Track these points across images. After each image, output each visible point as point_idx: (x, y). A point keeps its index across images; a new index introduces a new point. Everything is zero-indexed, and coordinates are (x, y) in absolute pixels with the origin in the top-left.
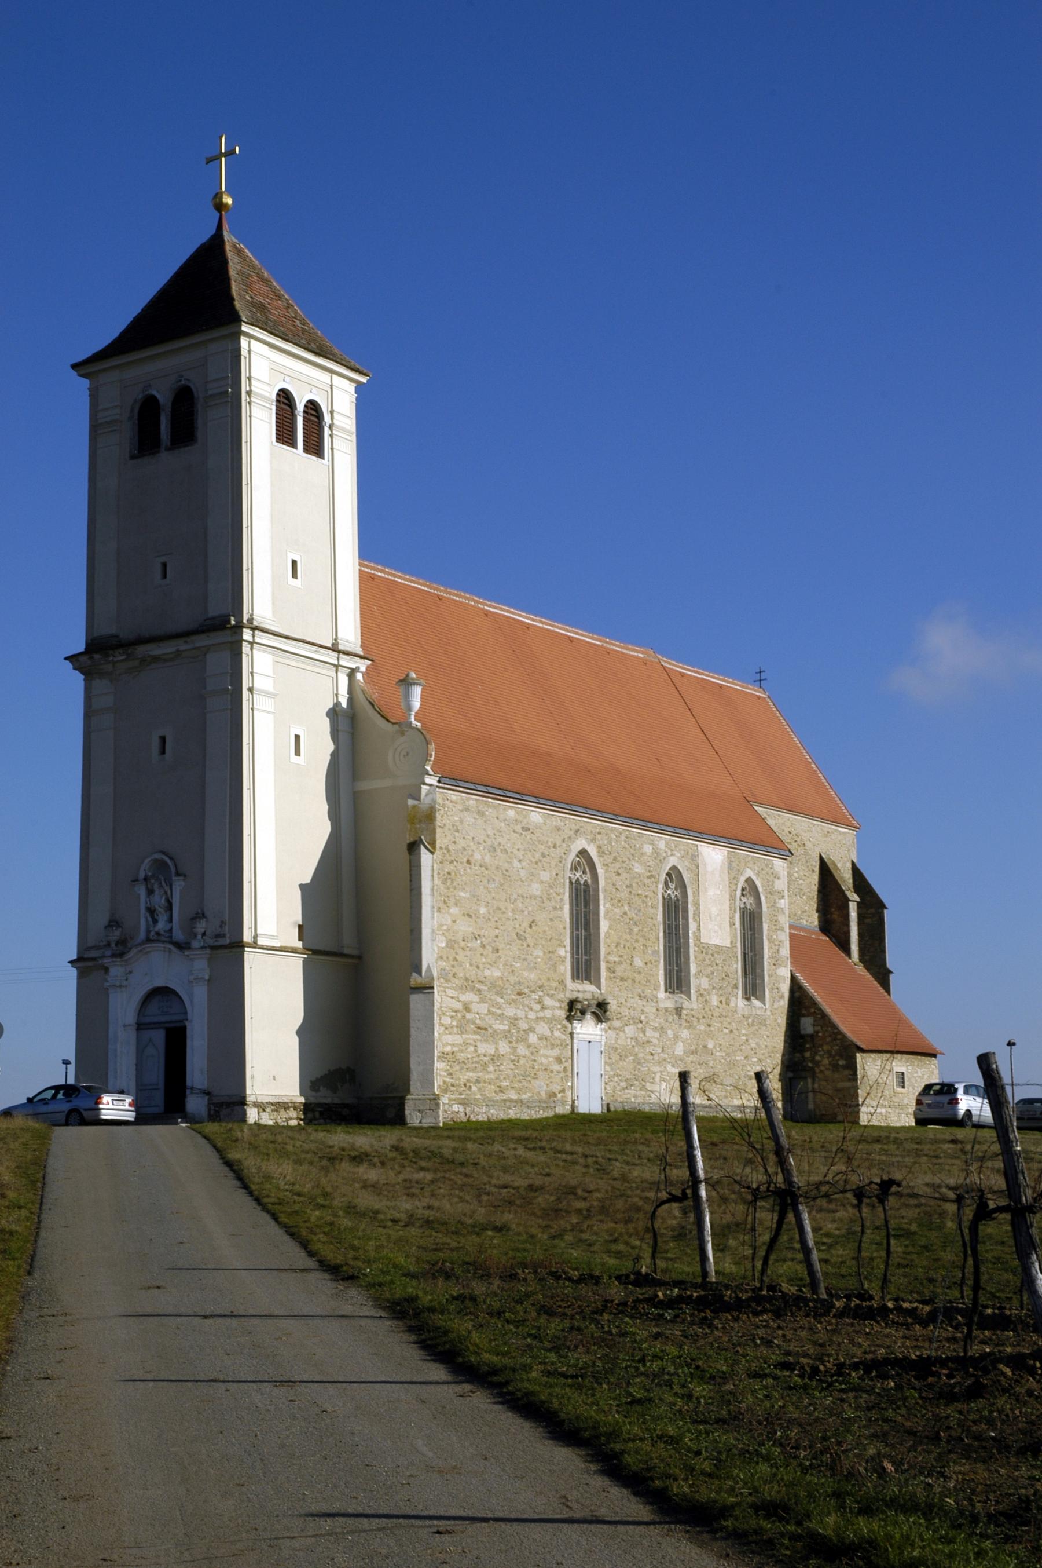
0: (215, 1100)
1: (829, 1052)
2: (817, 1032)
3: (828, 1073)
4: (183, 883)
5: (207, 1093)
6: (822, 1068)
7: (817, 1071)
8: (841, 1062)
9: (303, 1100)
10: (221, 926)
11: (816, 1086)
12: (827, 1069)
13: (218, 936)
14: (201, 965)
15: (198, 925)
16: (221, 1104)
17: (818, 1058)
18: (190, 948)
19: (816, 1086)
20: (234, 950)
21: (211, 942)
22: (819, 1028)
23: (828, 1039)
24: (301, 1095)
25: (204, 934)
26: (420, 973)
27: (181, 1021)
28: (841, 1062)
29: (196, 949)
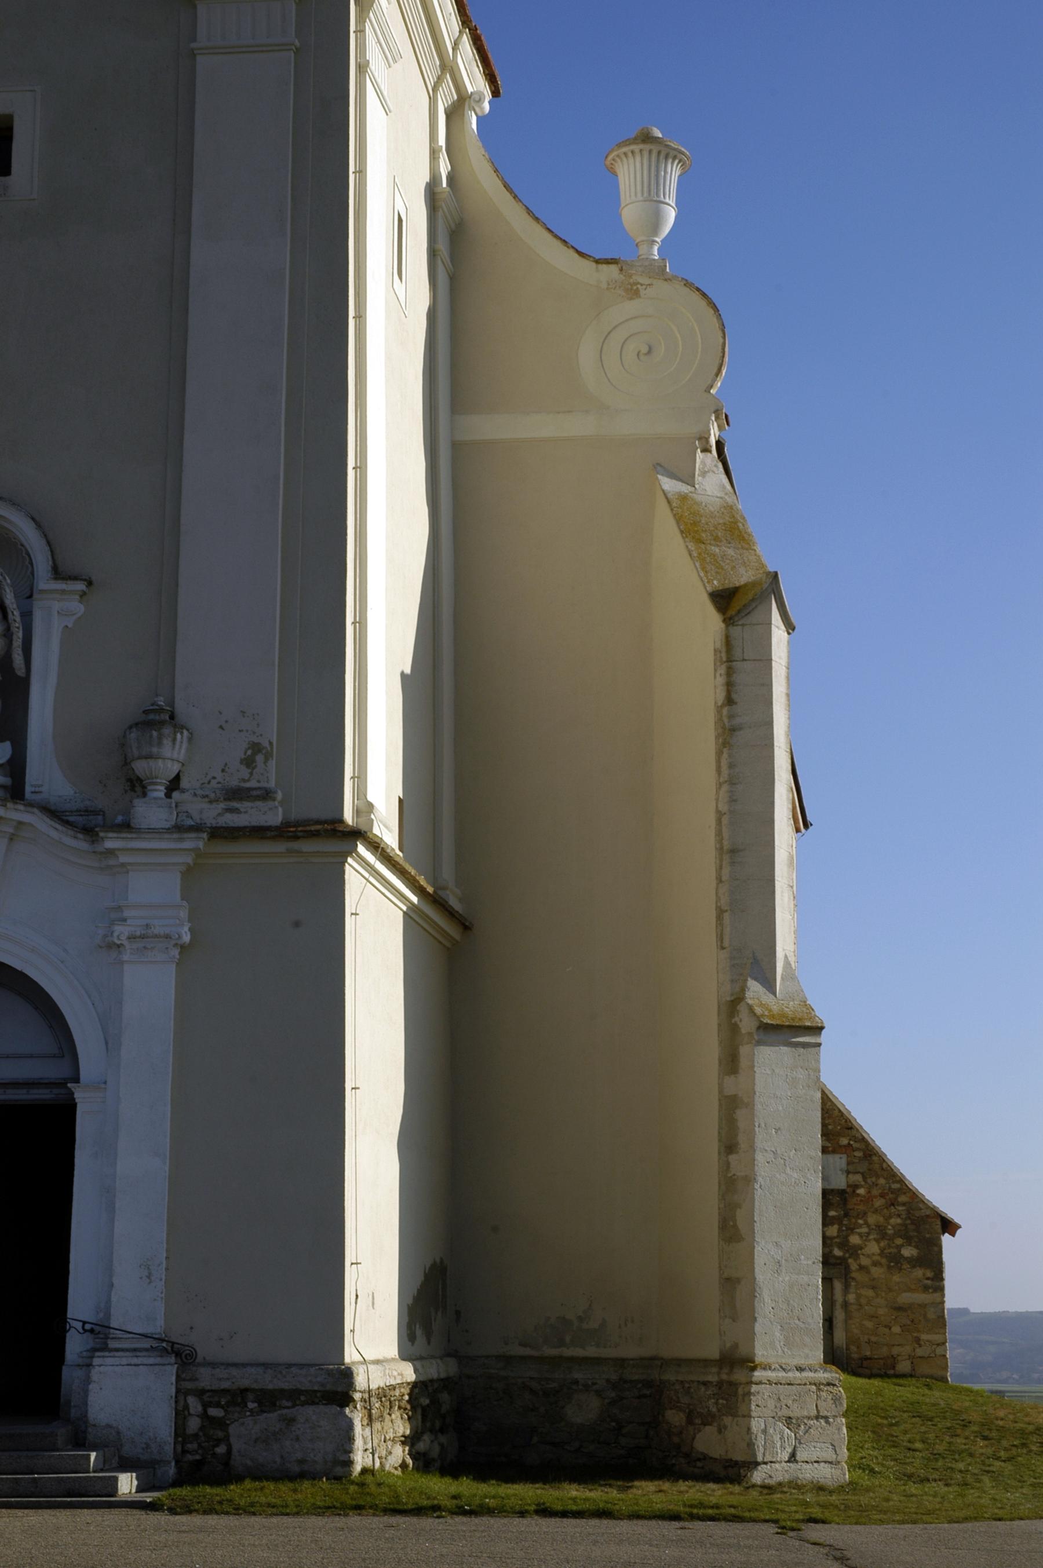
0: (206, 1379)
1: (881, 1230)
2: (856, 1186)
3: (877, 1272)
4: (78, 608)
5: (181, 1355)
6: (865, 1261)
7: (853, 1265)
8: (908, 1252)
9: (408, 1373)
10: (249, 762)
11: (851, 1298)
12: (875, 1264)
13: (236, 794)
14: (153, 886)
15: (167, 750)
16: (237, 1397)
17: (855, 1240)
18: (126, 826)
19: (851, 1298)
20: (307, 846)
21: (212, 814)
22: (858, 1178)
23: (879, 1203)
24: (404, 1356)
25: (174, 784)
26: (769, 984)
27: (62, 1084)
28: (908, 1252)
29: (154, 832)
